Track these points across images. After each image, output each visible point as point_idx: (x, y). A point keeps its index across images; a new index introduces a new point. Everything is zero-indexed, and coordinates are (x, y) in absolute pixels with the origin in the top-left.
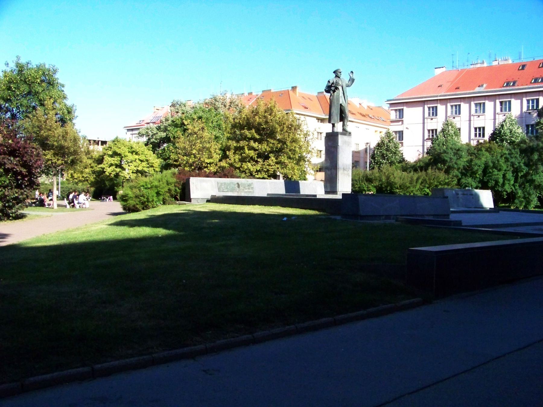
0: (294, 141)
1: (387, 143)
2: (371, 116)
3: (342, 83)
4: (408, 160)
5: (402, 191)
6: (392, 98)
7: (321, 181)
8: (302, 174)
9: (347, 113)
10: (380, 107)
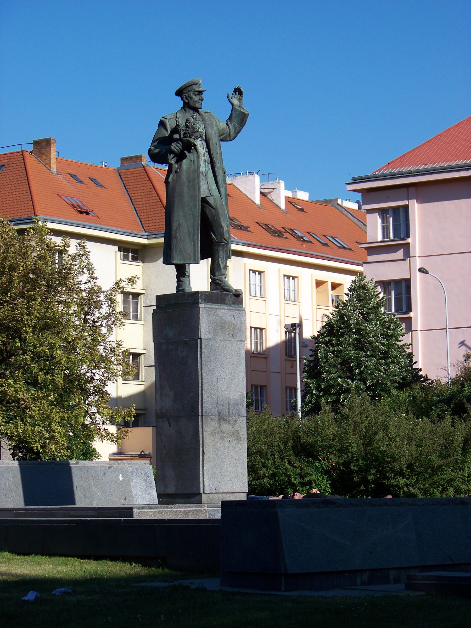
0: (47, 327)
1: (358, 324)
2: (300, 234)
3: (206, 129)
4: (432, 376)
5: (417, 482)
6: (369, 173)
7: (142, 456)
8: (76, 436)
9: (225, 228)
10: (331, 201)
